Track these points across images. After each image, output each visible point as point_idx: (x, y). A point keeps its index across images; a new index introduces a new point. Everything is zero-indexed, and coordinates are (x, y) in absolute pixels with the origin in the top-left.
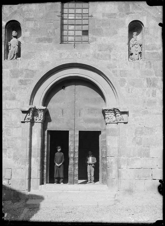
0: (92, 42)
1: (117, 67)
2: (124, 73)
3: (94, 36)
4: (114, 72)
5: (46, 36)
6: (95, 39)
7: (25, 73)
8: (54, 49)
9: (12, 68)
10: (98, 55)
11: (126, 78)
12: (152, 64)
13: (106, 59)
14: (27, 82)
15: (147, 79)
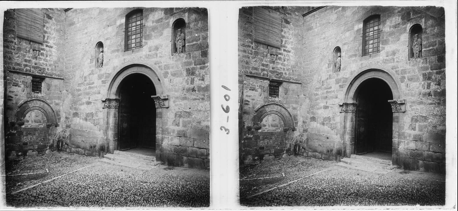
0: (381, 51)
1: (162, 62)
4: (159, 67)
11: (406, 76)
12: (192, 55)
13: (391, 63)
14: (344, 86)
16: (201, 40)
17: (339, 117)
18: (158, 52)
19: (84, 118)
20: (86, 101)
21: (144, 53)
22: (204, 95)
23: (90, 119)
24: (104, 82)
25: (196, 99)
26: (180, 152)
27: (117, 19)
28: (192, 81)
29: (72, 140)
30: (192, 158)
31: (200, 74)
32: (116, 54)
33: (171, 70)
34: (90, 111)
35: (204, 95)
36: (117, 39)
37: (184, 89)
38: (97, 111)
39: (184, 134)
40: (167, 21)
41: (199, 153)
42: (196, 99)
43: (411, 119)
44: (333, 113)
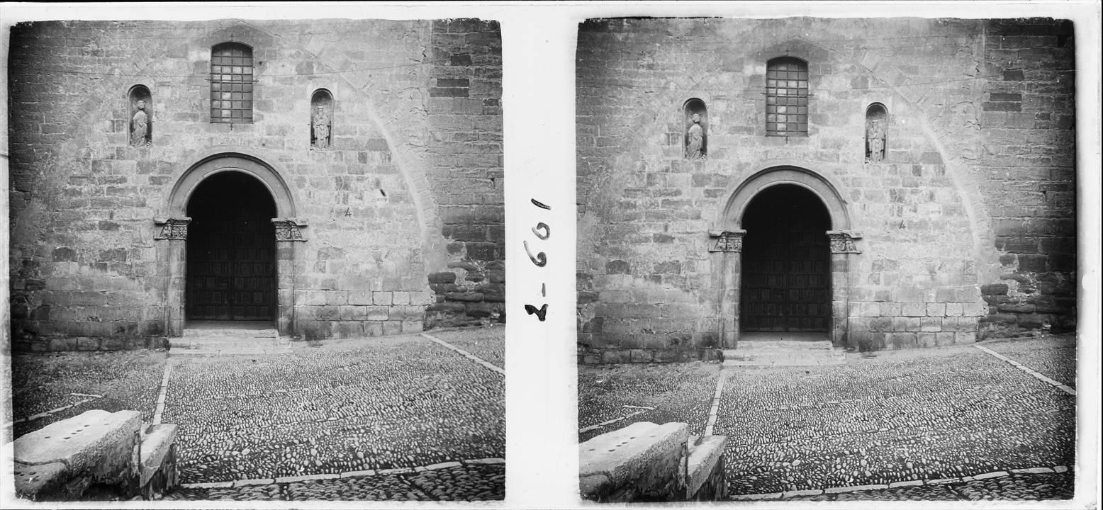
2: (856, 182)
3: (262, 113)
5: (189, 112)
6: (817, 131)
7: (713, 179)
8: (757, 144)
9: (138, 160)
10: (822, 153)
12: (898, 170)
15: (336, 178)
16: (357, 135)
17: (708, 261)
18: (840, 153)
19: (648, 274)
20: (654, 235)
21: (256, 134)
22: (917, 235)
23: (670, 278)
24: (712, 194)
25: (351, 228)
26: (327, 315)
27: (190, 47)
28: (900, 211)
29: (604, 330)
30: (899, 334)
31: (911, 201)
32: (744, 137)
33: (865, 188)
34: (116, 245)
35: (917, 235)
36: (191, 91)
37: (332, 211)
38: (137, 247)
39: (887, 297)
40: (856, 100)
41: (909, 325)
42: (351, 228)
43: (316, 254)
44: (134, 241)
